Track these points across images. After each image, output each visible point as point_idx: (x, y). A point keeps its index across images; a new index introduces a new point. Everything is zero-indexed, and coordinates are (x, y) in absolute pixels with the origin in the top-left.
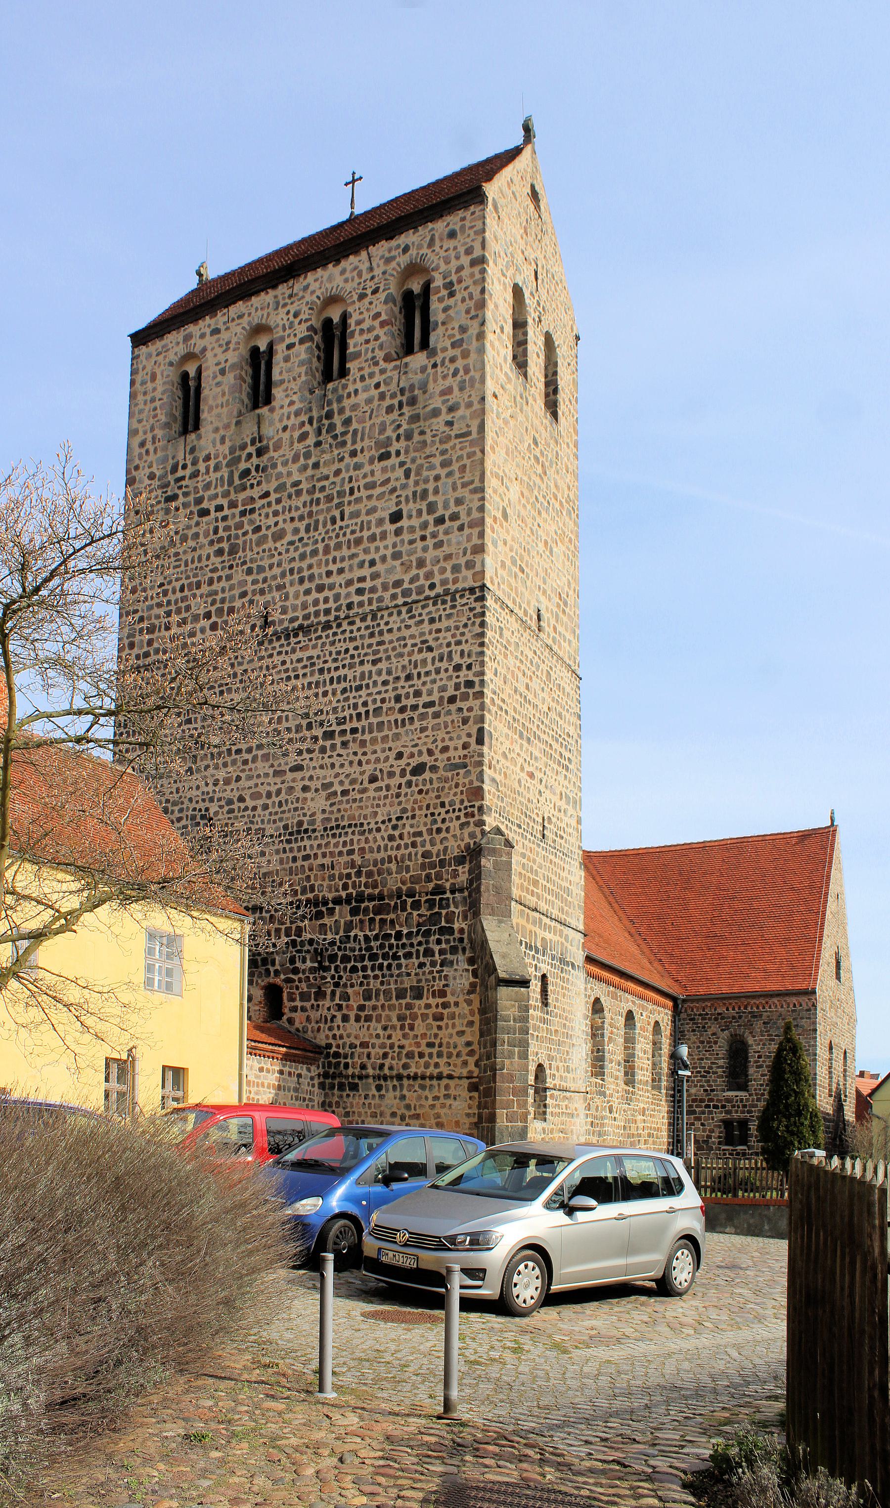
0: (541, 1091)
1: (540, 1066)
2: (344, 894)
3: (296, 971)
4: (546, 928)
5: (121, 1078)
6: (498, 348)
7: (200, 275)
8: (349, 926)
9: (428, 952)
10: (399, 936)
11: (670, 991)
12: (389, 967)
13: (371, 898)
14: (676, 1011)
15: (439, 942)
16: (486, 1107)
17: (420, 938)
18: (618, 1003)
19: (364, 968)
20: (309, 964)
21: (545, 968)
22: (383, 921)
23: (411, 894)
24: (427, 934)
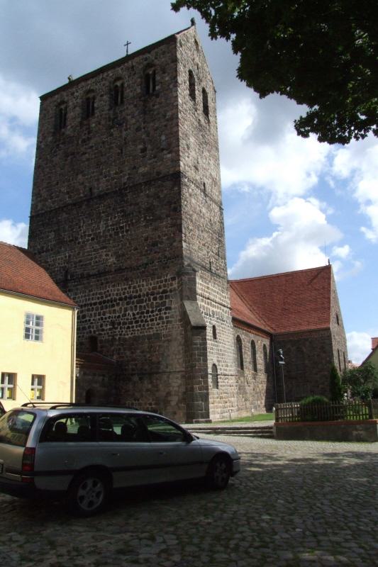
0: (216, 376)
1: (214, 365)
2: (123, 296)
3: (103, 330)
4: (214, 306)
5: (39, 384)
6: (183, 92)
7: (69, 78)
8: (126, 310)
9: (161, 318)
10: (148, 312)
11: (267, 329)
12: (144, 326)
13: (135, 297)
14: (271, 341)
15: (165, 313)
16: (189, 385)
17: (157, 312)
18: (246, 338)
19: (133, 327)
20: (108, 327)
21: (214, 323)
22: (141, 307)
23: (152, 294)
24: (160, 310)
